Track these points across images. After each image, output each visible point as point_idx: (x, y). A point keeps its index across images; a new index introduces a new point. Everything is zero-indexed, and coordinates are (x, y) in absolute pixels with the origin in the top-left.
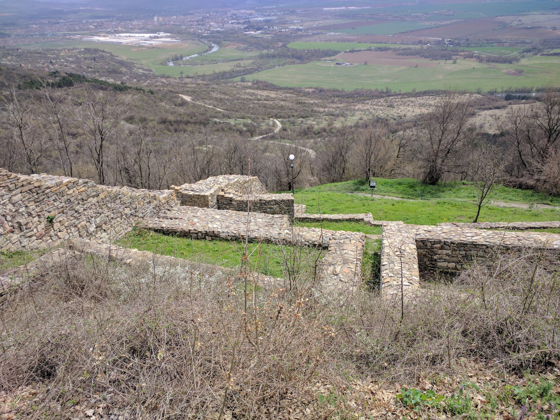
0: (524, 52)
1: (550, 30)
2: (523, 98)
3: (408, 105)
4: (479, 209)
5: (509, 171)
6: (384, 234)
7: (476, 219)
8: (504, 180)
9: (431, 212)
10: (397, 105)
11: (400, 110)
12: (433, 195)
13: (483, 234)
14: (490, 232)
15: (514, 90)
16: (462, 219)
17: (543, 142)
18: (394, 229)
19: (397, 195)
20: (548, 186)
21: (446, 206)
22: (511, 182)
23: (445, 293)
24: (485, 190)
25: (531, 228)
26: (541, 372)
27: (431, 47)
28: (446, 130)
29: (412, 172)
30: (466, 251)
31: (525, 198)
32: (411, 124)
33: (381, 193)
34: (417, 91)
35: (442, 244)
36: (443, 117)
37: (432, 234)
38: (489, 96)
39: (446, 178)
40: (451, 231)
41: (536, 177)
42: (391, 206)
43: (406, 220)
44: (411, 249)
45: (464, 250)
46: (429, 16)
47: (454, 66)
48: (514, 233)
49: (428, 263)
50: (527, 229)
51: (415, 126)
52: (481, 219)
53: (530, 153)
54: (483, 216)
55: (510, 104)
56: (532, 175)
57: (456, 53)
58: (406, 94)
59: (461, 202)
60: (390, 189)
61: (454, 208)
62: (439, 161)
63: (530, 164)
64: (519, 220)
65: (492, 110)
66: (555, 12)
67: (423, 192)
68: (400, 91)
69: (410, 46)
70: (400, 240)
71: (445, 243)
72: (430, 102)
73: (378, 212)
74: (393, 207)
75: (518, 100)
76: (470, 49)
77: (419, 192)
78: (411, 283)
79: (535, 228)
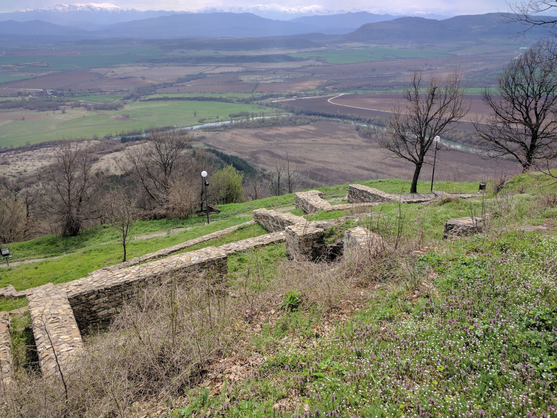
0: (125, 99)
1: (141, 80)
2: (137, 139)
3: (26, 159)
4: (125, 247)
5: (141, 205)
6: (31, 304)
7: (125, 258)
8: (140, 215)
9: (79, 264)
10: (13, 161)
11: (17, 166)
12: (78, 246)
13: (133, 271)
14: (138, 267)
15: (127, 133)
16: (112, 261)
17: (162, 175)
18: (41, 295)
19: (38, 256)
20: (176, 212)
21: (93, 253)
22: (146, 216)
23: (107, 343)
24: (125, 229)
25: (173, 252)
26: (199, 383)
27: (34, 99)
28: (72, 179)
29: (49, 228)
30: (120, 293)
31: (162, 226)
32: (35, 179)
33: (18, 260)
34: (32, 144)
35: (96, 294)
36: (66, 167)
37: (83, 287)
38: (106, 141)
39: (86, 226)
40: (101, 278)
41: (165, 207)
42: (33, 271)
43: (56, 280)
44: (65, 310)
45: (119, 292)
46: (22, 67)
47: (64, 115)
48: (158, 262)
49: (88, 317)
50: (170, 253)
51: (40, 180)
52: (130, 256)
53: (155, 187)
54: (130, 253)
55: (127, 146)
56: (162, 205)
57: (62, 103)
58: (20, 149)
59: (106, 245)
60: (28, 252)
61: (101, 253)
62: (74, 211)
63: (158, 196)
64: (162, 247)
65: (113, 154)
66: (140, 64)
67: (66, 246)
68: (11, 146)
69: (9, 99)
70: (49, 306)
71: (99, 292)
72: (49, 154)
73: (21, 280)
74: (37, 271)
75: (132, 142)
76: (75, 99)
77: (62, 247)
78: (73, 346)
79: (176, 251)
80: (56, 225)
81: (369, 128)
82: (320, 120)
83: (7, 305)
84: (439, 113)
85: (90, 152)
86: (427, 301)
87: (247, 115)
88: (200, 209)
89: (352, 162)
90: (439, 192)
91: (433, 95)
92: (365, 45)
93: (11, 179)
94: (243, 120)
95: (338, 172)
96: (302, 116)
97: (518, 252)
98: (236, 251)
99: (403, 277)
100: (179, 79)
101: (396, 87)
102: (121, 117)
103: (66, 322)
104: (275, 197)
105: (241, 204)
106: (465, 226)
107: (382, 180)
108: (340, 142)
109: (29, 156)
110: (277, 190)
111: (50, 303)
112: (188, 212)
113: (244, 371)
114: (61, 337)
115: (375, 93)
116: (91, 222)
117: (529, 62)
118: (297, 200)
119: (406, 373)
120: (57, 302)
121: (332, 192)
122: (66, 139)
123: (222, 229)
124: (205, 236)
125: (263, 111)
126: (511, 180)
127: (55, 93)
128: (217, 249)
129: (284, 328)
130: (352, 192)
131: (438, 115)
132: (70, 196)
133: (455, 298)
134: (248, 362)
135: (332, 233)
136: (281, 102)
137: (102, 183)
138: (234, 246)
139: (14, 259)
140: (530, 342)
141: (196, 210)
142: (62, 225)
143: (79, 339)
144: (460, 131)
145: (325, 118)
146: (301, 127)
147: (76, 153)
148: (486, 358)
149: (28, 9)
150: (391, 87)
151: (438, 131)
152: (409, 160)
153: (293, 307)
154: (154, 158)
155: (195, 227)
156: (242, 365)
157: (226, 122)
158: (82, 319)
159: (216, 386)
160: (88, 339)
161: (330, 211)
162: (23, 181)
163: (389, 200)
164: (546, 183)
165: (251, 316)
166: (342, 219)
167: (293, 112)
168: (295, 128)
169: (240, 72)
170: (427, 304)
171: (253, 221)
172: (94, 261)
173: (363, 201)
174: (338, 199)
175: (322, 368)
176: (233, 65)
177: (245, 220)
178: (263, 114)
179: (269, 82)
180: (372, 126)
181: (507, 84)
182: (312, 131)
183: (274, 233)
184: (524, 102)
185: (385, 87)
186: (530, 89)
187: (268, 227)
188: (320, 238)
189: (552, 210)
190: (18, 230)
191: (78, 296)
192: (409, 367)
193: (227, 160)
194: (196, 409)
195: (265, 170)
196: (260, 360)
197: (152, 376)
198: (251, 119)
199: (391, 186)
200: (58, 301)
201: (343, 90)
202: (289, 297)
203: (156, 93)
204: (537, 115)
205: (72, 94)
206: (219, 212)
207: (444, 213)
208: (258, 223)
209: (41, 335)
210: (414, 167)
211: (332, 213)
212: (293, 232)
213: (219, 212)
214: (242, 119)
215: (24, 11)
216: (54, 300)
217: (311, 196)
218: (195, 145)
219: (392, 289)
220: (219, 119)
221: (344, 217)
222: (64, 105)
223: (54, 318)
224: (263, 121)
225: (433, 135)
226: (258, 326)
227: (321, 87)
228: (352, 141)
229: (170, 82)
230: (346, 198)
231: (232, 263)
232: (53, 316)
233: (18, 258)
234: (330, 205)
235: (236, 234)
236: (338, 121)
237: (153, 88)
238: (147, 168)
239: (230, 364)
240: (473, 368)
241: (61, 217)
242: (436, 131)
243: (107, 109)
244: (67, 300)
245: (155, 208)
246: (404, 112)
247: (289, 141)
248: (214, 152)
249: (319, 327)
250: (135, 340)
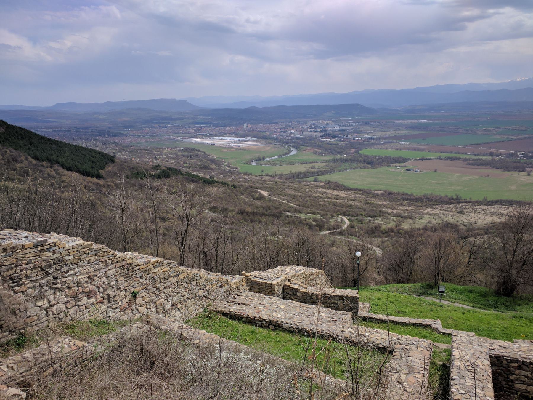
3: (479, 213)
6: (454, 344)
9: (506, 326)
10: (467, 212)
11: (470, 217)
12: (508, 307)
18: (465, 340)
19: (468, 304)
27: (503, 159)
33: (450, 300)
35: (520, 364)
37: (508, 350)
42: (460, 314)
44: (485, 365)
46: (501, 130)
47: (528, 177)
49: (504, 383)
51: (486, 233)
58: (477, 202)
60: (460, 296)
62: (514, 272)
69: (481, 157)
72: (502, 212)
73: (447, 319)
83: (432, 336)
93: (462, 227)
103: (483, 377)
109: (483, 210)
111: (472, 351)
127: (525, 156)
139: (448, 298)
142: (498, 282)
149: (523, 79)
162: (471, 231)
172: (522, 329)
182: (487, 230)
190: (456, 274)
209: (457, 377)
215: (519, 80)
233: (450, 298)
244: (488, 357)
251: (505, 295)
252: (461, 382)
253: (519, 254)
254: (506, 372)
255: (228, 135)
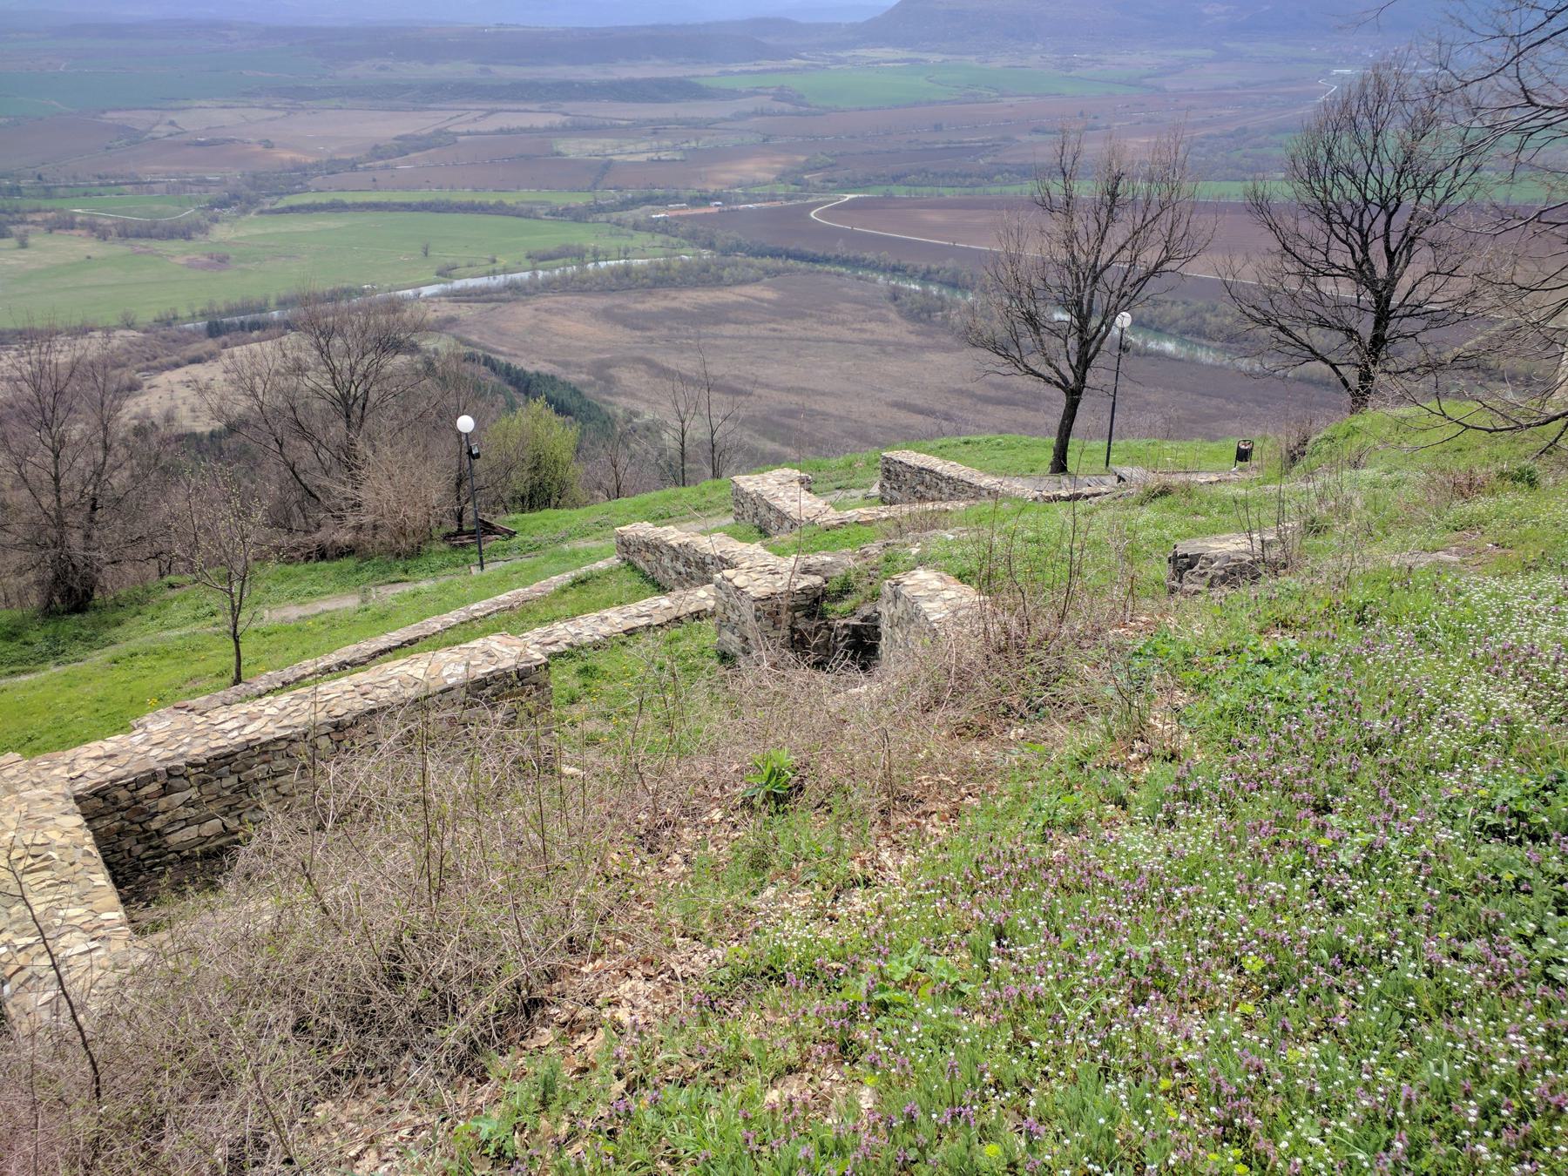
0: (212, 208)
1: (259, 148)
4: (237, 642)
5: (281, 520)
7: (238, 672)
8: (278, 549)
9: (100, 694)
12: (90, 642)
13: (270, 711)
14: (285, 698)
16: (200, 685)
20: (384, 536)
21: (141, 662)
22: (295, 549)
23: (222, 923)
24: (236, 589)
25: (382, 652)
31: (343, 580)
35: (162, 780)
37: (121, 761)
39: (114, 583)
40: (175, 733)
41: (352, 521)
43: (29, 745)
44: (69, 831)
45: (232, 773)
47: (25, 254)
48: (345, 682)
50: (373, 657)
52: (252, 669)
53: (316, 464)
55: (225, 346)
56: (339, 517)
59: (180, 638)
61: (167, 662)
62: (75, 539)
63: (326, 491)
64: (348, 640)
67: (57, 643)
75: (240, 334)
79: (390, 650)
80: (22, 581)
81: (925, 294)
82: (790, 270)
84: (1129, 246)
85: (117, 366)
86: (1174, 770)
87: (579, 255)
88: (455, 529)
89: (882, 391)
90: (1125, 471)
91: (1114, 195)
92: (913, 55)
94: (569, 270)
95: (841, 418)
96: (739, 257)
97: (1408, 623)
98: (571, 645)
99: (1090, 705)
100: (376, 147)
101: (998, 177)
102: (205, 259)
104: (671, 491)
105: (574, 512)
106: (1229, 559)
107: (972, 439)
108: (847, 334)
110: (677, 472)
112: (420, 538)
113: (657, 994)
114: (61, 913)
115: (940, 195)
116: (128, 568)
117: (1366, 107)
118: (740, 497)
119: (1148, 984)
120: (41, 810)
121: (833, 475)
122: (39, 324)
123: (525, 585)
124: (476, 606)
125: (624, 242)
126: (1326, 433)
128: (517, 641)
129: (759, 863)
130: (892, 473)
131: (1126, 253)
132: (63, 496)
133: (1256, 760)
134: (668, 968)
135: (845, 590)
136: (678, 217)
137: (157, 457)
138: (563, 632)
140: (1495, 877)
141: (442, 531)
142: (39, 583)
143: (118, 915)
144: (1173, 303)
145: (802, 265)
146: (737, 290)
147: (73, 368)
148: (1379, 930)
150: (988, 177)
151: (1124, 299)
152: (1048, 380)
153: (780, 799)
154: (309, 382)
155: (442, 581)
156: (648, 978)
157: (517, 276)
158: (119, 856)
159: (575, 1046)
160: (145, 916)
161: (834, 527)
163: (993, 494)
164: (1421, 439)
165: (654, 832)
166: (873, 549)
167: (711, 246)
168: (718, 293)
169: (556, 130)
170: (1178, 779)
171: (614, 560)
173: (922, 498)
174: (854, 492)
175: (897, 978)
176: (535, 107)
177: (590, 557)
178: (626, 253)
179: (643, 158)
180: (934, 290)
181: (1313, 169)
182: (769, 301)
183: (679, 592)
184: (1357, 217)
185: (970, 176)
186: (1372, 182)
187: (659, 575)
188: (813, 604)
189: (1468, 507)
191: (107, 788)
192: (1160, 964)
193: (525, 385)
194: (525, 1118)
195: (637, 414)
196: (702, 961)
197: (381, 1024)
198: (590, 266)
199: (998, 454)
200: (44, 805)
201: (852, 185)
202: (767, 772)
203: (306, 190)
204: (1390, 255)
205: (48, 189)
206: (512, 534)
207: (1155, 526)
208: (630, 564)
210: (1060, 400)
211: (839, 532)
212: (738, 588)
213: (512, 534)
214: (565, 265)
216: (31, 803)
217: (776, 486)
218: (429, 344)
219: (1067, 740)
220: (498, 267)
221: (879, 543)
222: (22, 222)
223: (34, 857)
224: (627, 271)
225: (1109, 315)
226: (676, 858)
227: (790, 176)
228: (879, 330)
229: (348, 157)
230: (875, 490)
231: (564, 679)
232: (33, 851)
234: (832, 510)
235: (568, 597)
236: (840, 275)
237: (298, 177)
238: (293, 409)
239: (614, 977)
240: (1346, 959)
241: (34, 557)
242: (1121, 297)
243: (159, 237)
245: (319, 526)
246: (1032, 251)
247: (703, 331)
248: (488, 362)
249: (865, 856)
250: (309, 918)
251: (71, 611)
252: (14, 917)
253: (72, 485)
254: (137, 819)
255: (461, 271)
